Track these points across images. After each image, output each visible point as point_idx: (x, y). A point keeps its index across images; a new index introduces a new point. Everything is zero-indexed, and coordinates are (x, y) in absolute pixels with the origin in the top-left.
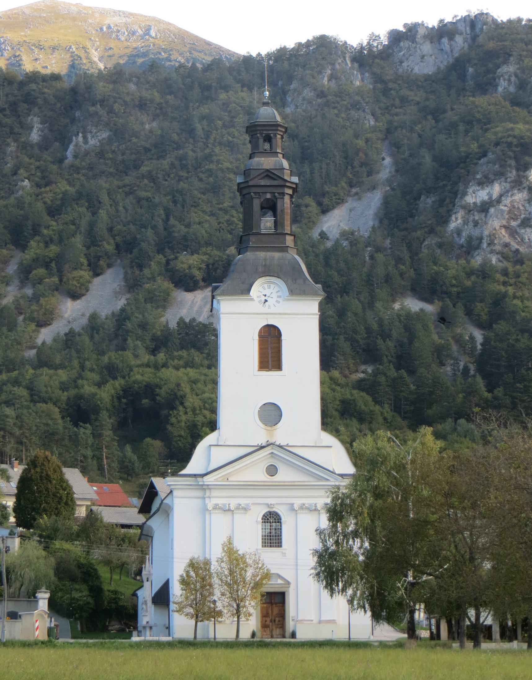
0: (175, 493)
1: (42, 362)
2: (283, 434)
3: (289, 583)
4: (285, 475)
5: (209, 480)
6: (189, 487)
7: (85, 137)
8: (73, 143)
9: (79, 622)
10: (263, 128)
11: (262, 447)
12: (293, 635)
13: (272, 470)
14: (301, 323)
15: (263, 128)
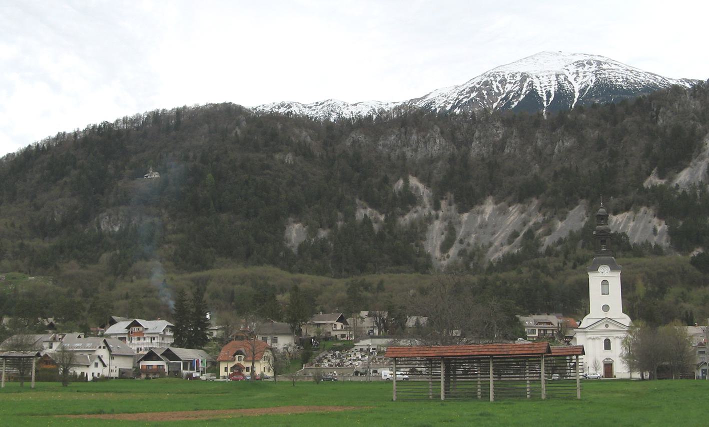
0: (577, 334)
1: (549, 252)
2: (609, 315)
3: (613, 361)
4: (611, 327)
5: (587, 330)
6: (581, 332)
7: (563, 142)
8: (558, 145)
9: (61, 350)
10: (519, 360)
11: (603, 319)
12: (615, 376)
13: (607, 326)
14: (615, 280)
15: (519, 360)
